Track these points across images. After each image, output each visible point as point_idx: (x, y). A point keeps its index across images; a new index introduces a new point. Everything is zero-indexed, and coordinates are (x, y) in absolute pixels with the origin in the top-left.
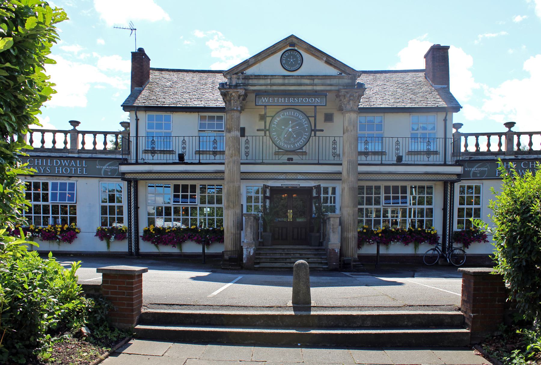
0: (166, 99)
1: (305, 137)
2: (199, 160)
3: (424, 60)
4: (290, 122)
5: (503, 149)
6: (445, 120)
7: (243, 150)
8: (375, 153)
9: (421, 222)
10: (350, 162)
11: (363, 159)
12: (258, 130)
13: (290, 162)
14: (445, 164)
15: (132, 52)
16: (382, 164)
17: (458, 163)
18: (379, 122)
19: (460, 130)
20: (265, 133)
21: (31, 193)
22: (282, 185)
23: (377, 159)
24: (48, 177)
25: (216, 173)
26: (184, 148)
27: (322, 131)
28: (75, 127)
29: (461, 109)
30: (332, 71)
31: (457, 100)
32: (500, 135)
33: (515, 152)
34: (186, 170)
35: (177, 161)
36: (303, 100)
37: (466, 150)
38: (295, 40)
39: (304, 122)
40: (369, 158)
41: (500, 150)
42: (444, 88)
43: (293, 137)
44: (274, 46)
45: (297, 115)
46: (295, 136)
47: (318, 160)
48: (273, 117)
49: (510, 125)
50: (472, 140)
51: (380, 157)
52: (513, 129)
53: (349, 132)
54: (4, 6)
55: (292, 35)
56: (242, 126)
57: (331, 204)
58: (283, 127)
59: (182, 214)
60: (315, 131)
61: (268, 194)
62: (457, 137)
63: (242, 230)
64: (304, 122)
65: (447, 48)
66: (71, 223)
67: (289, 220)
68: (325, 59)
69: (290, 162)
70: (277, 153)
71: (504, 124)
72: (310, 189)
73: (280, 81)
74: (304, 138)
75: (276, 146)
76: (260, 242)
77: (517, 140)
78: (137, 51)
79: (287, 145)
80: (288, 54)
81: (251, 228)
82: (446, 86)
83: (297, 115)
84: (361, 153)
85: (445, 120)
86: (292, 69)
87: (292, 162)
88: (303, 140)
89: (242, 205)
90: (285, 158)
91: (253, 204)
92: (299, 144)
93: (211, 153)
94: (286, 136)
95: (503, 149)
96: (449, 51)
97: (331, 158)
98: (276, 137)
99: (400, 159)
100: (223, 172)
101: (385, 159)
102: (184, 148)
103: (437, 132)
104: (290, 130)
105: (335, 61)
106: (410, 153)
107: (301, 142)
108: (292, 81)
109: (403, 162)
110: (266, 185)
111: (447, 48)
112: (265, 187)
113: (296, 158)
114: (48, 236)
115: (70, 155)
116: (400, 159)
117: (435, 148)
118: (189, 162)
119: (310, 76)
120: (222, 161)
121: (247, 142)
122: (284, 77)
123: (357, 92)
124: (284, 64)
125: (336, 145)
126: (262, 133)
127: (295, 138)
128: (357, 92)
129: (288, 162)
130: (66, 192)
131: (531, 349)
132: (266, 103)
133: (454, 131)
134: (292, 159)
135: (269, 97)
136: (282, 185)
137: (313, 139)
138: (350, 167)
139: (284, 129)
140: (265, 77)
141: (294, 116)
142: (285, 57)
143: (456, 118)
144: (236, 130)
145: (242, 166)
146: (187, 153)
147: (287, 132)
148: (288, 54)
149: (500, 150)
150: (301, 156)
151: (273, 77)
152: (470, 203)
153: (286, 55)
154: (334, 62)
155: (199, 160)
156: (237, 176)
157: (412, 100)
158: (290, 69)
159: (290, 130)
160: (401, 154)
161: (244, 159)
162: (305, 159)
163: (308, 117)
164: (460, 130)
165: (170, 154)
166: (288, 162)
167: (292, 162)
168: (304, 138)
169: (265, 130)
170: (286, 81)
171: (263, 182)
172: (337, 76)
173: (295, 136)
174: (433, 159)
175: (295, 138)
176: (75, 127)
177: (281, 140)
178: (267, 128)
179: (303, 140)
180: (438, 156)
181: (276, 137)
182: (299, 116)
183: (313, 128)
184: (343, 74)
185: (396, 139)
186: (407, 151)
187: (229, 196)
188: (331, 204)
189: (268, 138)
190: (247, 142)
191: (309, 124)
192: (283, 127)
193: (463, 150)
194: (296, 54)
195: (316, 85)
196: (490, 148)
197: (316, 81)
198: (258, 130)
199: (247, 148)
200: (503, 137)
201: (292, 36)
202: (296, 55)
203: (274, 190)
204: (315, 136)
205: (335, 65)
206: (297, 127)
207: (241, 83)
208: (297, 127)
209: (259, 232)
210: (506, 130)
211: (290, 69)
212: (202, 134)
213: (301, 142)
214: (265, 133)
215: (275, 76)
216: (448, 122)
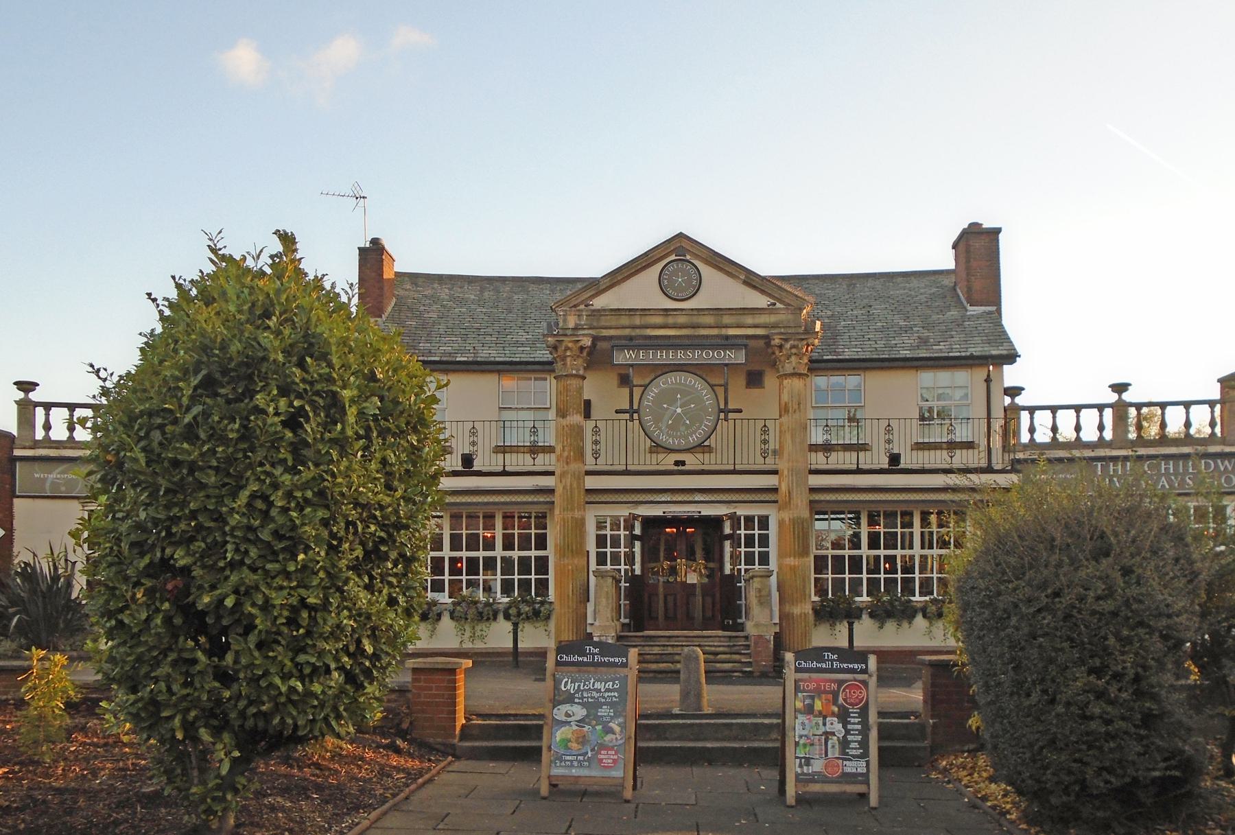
0: (433, 345)
1: (708, 423)
2: (504, 466)
3: (951, 253)
4: (679, 396)
6: (988, 380)
7: (589, 448)
8: (847, 448)
9: (891, 583)
10: (792, 470)
11: (819, 460)
12: (617, 412)
13: (680, 469)
14: (989, 470)
15: (359, 248)
16: (859, 471)
17: (1014, 466)
18: (855, 387)
19: (1019, 400)
20: (632, 416)
21: (845, 578)
22: (664, 513)
23: (847, 460)
26: (474, 444)
27: (740, 411)
29: (1018, 358)
30: (760, 301)
31: (1012, 339)
32: (1101, 408)
33: (1132, 442)
35: (460, 468)
36: (702, 353)
37: (1032, 439)
38: (685, 244)
39: (705, 395)
40: (834, 456)
41: (1101, 438)
42: (990, 313)
43: (685, 424)
44: (646, 254)
45: (691, 381)
46: (688, 422)
47: (735, 464)
48: (646, 387)
49: (1120, 388)
50: (1043, 418)
51: (854, 454)
52: (1126, 397)
53: (790, 415)
54: (917, 721)
55: (681, 233)
56: (586, 398)
58: (665, 406)
59: (885, 568)
60: (726, 411)
61: (637, 531)
62: (1012, 412)
63: (588, 601)
64: (705, 395)
65: (997, 231)
67: (679, 579)
68: (743, 277)
69: (680, 468)
70: (653, 449)
71: (1110, 387)
72: (717, 522)
73: (658, 320)
74: (706, 426)
75: (646, 434)
76: (623, 625)
78: (368, 245)
79: (673, 440)
80: (673, 267)
81: (607, 598)
82: (994, 308)
83: (691, 381)
84: (814, 448)
85: (988, 380)
86: (681, 296)
87: (683, 468)
88: (703, 430)
89: (588, 552)
90: (668, 461)
91: (609, 550)
92: (697, 437)
94: (670, 422)
95: (1108, 435)
96: (1001, 236)
97: (760, 460)
98: (652, 425)
99: (894, 459)
100: (551, 491)
101: (866, 460)
102: (474, 444)
104: (679, 410)
105: (762, 280)
106: (919, 446)
107: (700, 434)
108: (682, 320)
109: (902, 466)
110: (634, 514)
111: (997, 231)
112: (635, 517)
113: (691, 461)
114: (999, 542)
116: (894, 459)
117: (970, 434)
118: (485, 469)
119: (716, 309)
120: (551, 469)
121: (596, 430)
122: (666, 312)
123: (803, 339)
124: (665, 286)
125: (762, 449)
126: (627, 416)
127: (688, 427)
128: (803, 339)
129: (676, 468)
131: (933, 706)
132: (633, 360)
133: (1008, 400)
134: (683, 463)
135: (638, 350)
136: (664, 513)
137: (722, 425)
138: (792, 480)
139: (667, 409)
140: (631, 312)
141: (685, 385)
142: (667, 274)
143: (1011, 375)
144: (576, 413)
145: (587, 478)
146: (480, 453)
147: (673, 415)
148: (673, 267)
149: (1101, 438)
150: (700, 456)
151: (645, 312)
153: (669, 271)
154: (760, 282)
155: (504, 466)
156: (580, 497)
157: (924, 341)
158: (677, 296)
159: (679, 410)
160: (896, 451)
161: (590, 463)
162: (709, 461)
163: (712, 386)
164: (1019, 400)
166: (676, 468)
167: (683, 468)
168: (706, 426)
169: (631, 411)
170: (670, 320)
171: (628, 508)
172: (766, 309)
173: (688, 422)
174: (961, 458)
175: (688, 427)
177: (662, 431)
178: (635, 407)
179: (703, 430)
180: (976, 451)
181: (652, 425)
182: (695, 383)
183: (722, 406)
184: (778, 305)
185: (884, 424)
187: (564, 537)
189: (637, 422)
190: (596, 430)
191: (715, 399)
192: (665, 406)
193: (1025, 437)
194: (689, 267)
195: (726, 327)
196: (1082, 435)
197: (727, 320)
198: (617, 412)
199: (596, 442)
200: (1108, 413)
201: (681, 236)
202: (689, 269)
203: (648, 522)
204: (726, 419)
205: (762, 288)
206: (693, 406)
207: (585, 325)
208: (693, 406)
209: (620, 605)
210: (1113, 398)
211: (677, 296)
212: (507, 415)
213: (700, 434)
214: (632, 416)
215: (649, 310)
216: (993, 385)
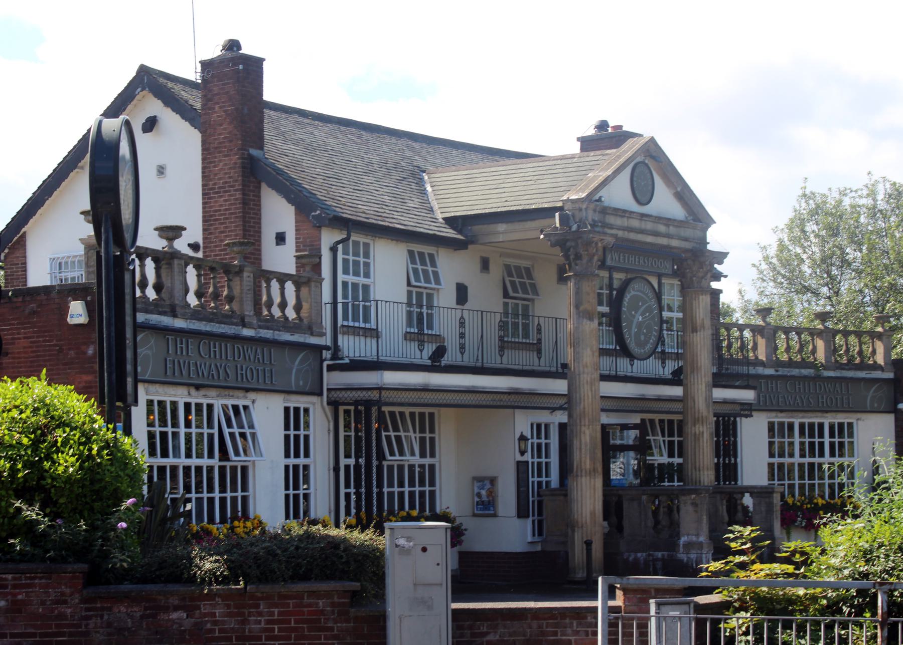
2: (378, 356)
5: (762, 357)
24: (790, 414)
25: (509, 393)
28: (171, 240)
34: (473, 387)
57: (671, 460)
66: (232, 522)
70: (408, 336)
77: (294, 294)
93: (674, 356)
103: (374, 283)
115: (286, 337)
130: (676, 435)
152: (781, 455)
155: (378, 356)
165: (366, 337)
176: (171, 240)
186: (404, 332)
188: (671, 460)
